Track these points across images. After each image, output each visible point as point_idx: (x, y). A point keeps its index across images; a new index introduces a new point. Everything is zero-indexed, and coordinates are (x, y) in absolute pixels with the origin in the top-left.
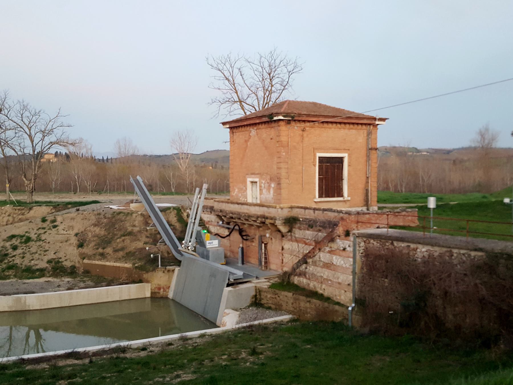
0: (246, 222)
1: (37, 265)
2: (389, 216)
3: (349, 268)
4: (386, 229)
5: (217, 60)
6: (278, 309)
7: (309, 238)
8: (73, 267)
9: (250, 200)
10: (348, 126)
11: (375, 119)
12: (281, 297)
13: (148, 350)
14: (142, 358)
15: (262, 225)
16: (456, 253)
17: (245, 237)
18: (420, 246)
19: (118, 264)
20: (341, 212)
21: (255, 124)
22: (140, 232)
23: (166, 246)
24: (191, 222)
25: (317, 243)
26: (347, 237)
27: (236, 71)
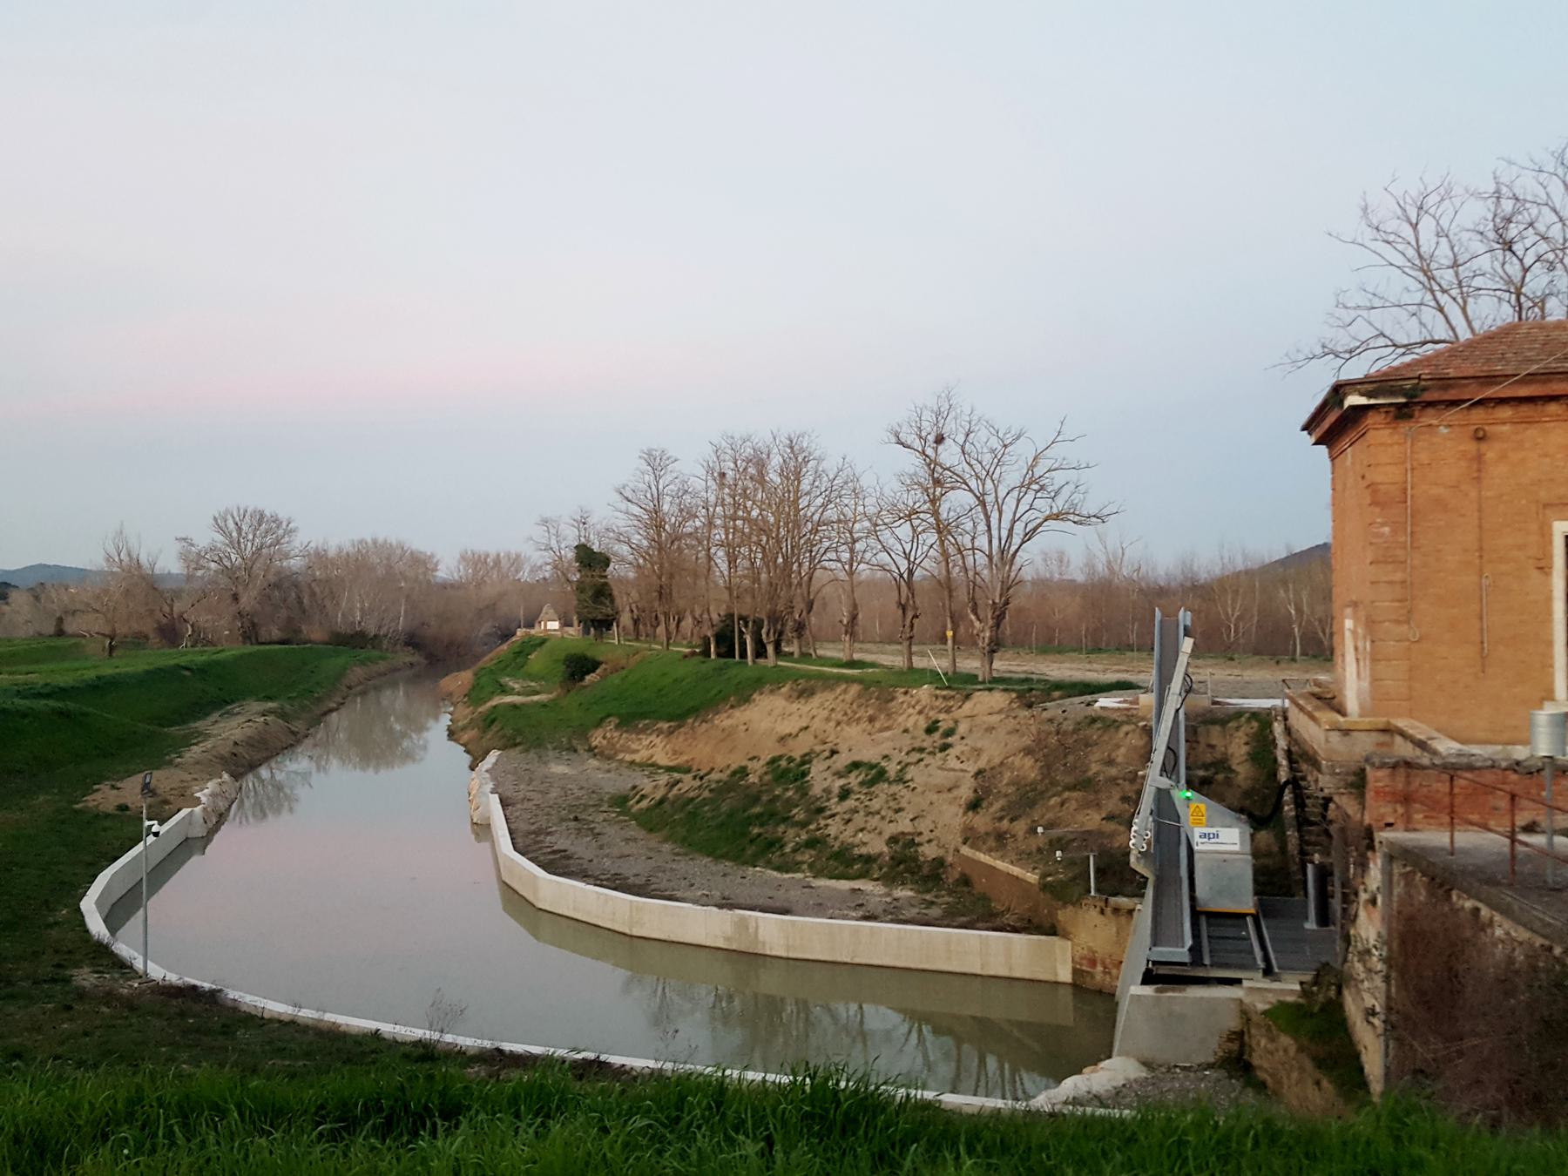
1: (865, 844)
8: (940, 862)
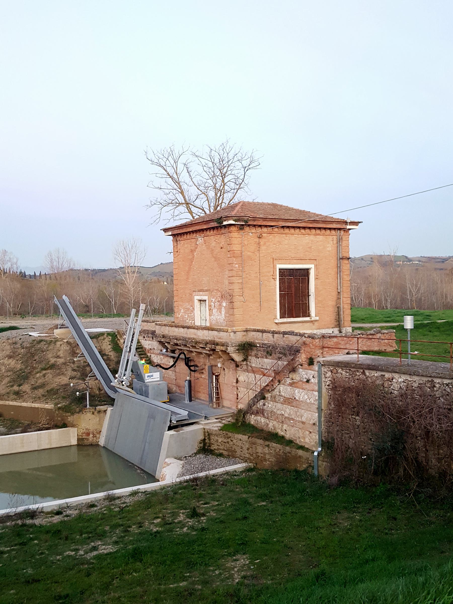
0: (193, 350)
2: (360, 340)
3: (314, 404)
4: (356, 356)
5: (158, 154)
6: (231, 455)
7: (268, 368)
9: (198, 323)
10: (313, 231)
11: (346, 223)
12: (235, 441)
13: (64, 514)
14: (54, 525)
15: (212, 353)
16: (439, 383)
17: (192, 368)
18: (396, 376)
19: (36, 405)
20: (302, 335)
21: (202, 230)
22: (65, 364)
23: (97, 381)
24: (126, 351)
25: (277, 373)
26: (311, 366)
27: (180, 167)
